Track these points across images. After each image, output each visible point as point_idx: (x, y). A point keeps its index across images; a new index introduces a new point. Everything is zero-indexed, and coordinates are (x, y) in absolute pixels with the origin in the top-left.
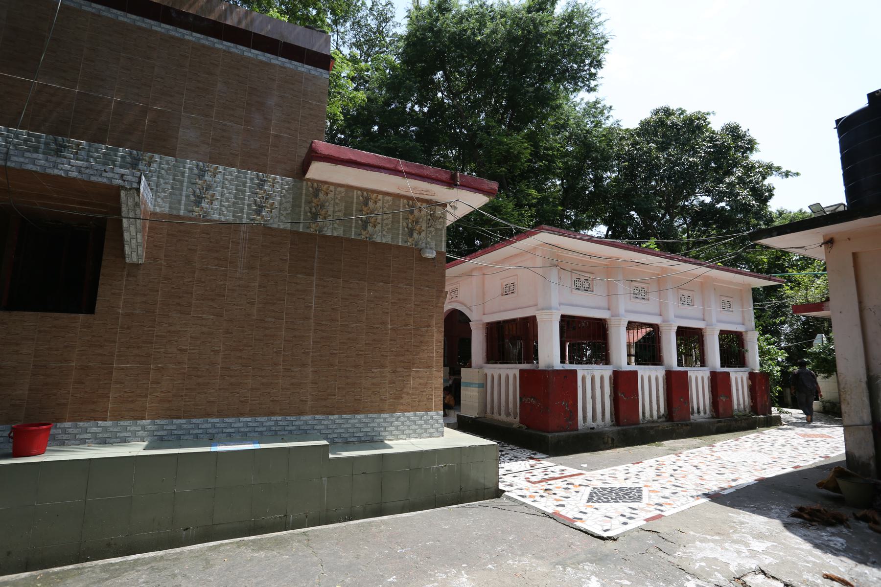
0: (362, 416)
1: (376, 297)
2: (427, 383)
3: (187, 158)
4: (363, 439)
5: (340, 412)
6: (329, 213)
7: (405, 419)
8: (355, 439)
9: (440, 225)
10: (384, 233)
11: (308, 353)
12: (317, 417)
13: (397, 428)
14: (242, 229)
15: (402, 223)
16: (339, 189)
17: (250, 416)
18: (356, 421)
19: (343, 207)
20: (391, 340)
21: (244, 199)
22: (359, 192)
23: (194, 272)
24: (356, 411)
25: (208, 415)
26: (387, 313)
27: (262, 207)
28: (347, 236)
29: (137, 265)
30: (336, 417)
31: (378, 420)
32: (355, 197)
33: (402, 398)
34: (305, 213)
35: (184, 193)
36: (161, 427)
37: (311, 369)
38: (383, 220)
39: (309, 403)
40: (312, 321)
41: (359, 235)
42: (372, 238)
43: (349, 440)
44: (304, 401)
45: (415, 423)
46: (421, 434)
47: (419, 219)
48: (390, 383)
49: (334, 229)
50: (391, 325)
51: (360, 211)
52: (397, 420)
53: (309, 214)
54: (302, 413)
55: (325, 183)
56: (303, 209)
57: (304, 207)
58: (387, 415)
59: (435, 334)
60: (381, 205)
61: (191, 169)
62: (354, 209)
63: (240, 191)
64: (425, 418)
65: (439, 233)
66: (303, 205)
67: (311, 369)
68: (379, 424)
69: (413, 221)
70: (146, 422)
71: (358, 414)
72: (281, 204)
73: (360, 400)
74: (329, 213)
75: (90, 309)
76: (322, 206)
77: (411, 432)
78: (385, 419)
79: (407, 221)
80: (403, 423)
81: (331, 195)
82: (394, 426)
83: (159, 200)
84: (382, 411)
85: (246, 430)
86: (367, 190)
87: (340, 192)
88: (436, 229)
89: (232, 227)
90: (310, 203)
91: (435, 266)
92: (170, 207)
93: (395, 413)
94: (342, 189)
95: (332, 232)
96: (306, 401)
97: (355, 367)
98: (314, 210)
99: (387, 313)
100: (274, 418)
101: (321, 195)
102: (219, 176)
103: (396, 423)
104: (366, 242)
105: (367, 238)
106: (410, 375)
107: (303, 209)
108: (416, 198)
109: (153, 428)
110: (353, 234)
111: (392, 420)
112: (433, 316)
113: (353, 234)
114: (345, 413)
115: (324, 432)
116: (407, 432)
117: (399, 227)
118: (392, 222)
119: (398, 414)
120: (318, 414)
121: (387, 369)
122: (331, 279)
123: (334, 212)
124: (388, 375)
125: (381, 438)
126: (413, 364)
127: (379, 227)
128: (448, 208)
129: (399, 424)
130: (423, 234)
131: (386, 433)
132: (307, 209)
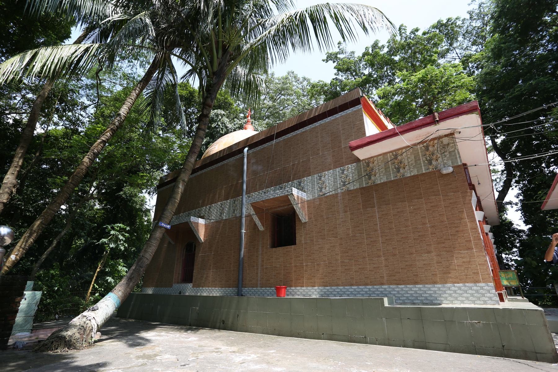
0: (421, 286)
1: (415, 209)
2: (470, 261)
3: (315, 174)
4: (425, 302)
5: (405, 283)
6: (406, 164)
7: (456, 289)
8: (419, 302)
9: (452, 148)
10: (411, 170)
11: (380, 250)
12: (391, 286)
13: (450, 295)
14: (339, 195)
15: (391, 167)
16: (379, 157)
17: (356, 285)
18: (302, 291)
19: (413, 158)
20: (431, 234)
21: (337, 182)
22: (391, 154)
23: (324, 220)
24: (416, 283)
25: (366, 284)
26: (392, 222)
27: (322, 188)
28: (420, 173)
29: (305, 223)
30: (403, 286)
31: (433, 289)
32: (389, 157)
33: (450, 273)
34: (424, 162)
35: (338, 183)
36: (321, 290)
37: (383, 258)
38: (379, 170)
39: (385, 278)
40: (379, 232)
41: (368, 184)
42: (404, 175)
43: (414, 302)
44: (382, 277)
45: (466, 292)
46: (474, 301)
47: (402, 160)
48: (437, 263)
49: (354, 185)
50: (429, 224)
51: (425, 155)
52: (449, 289)
53: (426, 162)
54: (382, 284)
55: (372, 157)
56: (421, 160)
57: (232, 209)
58: (440, 286)
59: (468, 224)
60: (377, 163)
61: (339, 172)
62: (421, 156)
63: (335, 179)
64: (475, 288)
65: (453, 154)
66: (421, 158)
67: (383, 258)
68: (435, 292)
69: (430, 155)
70: (316, 288)
71: (418, 284)
72: (353, 177)
73: (417, 275)
74: (406, 164)
75: (294, 243)
76: (401, 162)
77: (464, 299)
78: (439, 288)
79: (394, 165)
80: (455, 292)
81: (376, 162)
82: (447, 294)
83: (309, 195)
84: (435, 283)
85: (356, 293)
86: (395, 151)
87: (380, 159)
88: (450, 152)
89: (335, 196)
90: (425, 155)
91: (455, 177)
92: (312, 196)
93: (446, 284)
94: (381, 157)
95: (410, 174)
96: (383, 277)
97: (468, 250)
98: (428, 158)
99: (425, 217)
100: (368, 287)
101: (371, 165)
102: (327, 176)
103: (448, 292)
104: (401, 179)
105: (433, 169)
106: (453, 256)
107: (421, 160)
108: (412, 145)
109: (319, 291)
110: (364, 184)
111: (444, 289)
112: (463, 212)
113: (364, 184)
114: (409, 284)
115: (397, 295)
116: (460, 298)
117: (421, 162)
118: (415, 161)
119: (449, 285)
120: (391, 284)
121: (434, 254)
122: (401, 203)
123: (408, 162)
124: (435, 257)
125: (439, 302)
126: (454, 248)
127: (407, 168)
128: (456, 135)
129: (452, 292)
130: (440, 160)
131: (442, 299)
132: (424, 159)
